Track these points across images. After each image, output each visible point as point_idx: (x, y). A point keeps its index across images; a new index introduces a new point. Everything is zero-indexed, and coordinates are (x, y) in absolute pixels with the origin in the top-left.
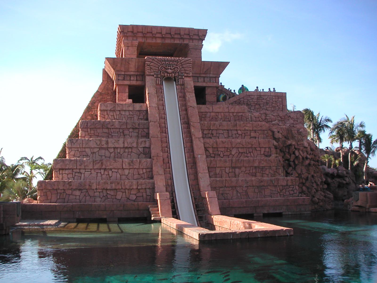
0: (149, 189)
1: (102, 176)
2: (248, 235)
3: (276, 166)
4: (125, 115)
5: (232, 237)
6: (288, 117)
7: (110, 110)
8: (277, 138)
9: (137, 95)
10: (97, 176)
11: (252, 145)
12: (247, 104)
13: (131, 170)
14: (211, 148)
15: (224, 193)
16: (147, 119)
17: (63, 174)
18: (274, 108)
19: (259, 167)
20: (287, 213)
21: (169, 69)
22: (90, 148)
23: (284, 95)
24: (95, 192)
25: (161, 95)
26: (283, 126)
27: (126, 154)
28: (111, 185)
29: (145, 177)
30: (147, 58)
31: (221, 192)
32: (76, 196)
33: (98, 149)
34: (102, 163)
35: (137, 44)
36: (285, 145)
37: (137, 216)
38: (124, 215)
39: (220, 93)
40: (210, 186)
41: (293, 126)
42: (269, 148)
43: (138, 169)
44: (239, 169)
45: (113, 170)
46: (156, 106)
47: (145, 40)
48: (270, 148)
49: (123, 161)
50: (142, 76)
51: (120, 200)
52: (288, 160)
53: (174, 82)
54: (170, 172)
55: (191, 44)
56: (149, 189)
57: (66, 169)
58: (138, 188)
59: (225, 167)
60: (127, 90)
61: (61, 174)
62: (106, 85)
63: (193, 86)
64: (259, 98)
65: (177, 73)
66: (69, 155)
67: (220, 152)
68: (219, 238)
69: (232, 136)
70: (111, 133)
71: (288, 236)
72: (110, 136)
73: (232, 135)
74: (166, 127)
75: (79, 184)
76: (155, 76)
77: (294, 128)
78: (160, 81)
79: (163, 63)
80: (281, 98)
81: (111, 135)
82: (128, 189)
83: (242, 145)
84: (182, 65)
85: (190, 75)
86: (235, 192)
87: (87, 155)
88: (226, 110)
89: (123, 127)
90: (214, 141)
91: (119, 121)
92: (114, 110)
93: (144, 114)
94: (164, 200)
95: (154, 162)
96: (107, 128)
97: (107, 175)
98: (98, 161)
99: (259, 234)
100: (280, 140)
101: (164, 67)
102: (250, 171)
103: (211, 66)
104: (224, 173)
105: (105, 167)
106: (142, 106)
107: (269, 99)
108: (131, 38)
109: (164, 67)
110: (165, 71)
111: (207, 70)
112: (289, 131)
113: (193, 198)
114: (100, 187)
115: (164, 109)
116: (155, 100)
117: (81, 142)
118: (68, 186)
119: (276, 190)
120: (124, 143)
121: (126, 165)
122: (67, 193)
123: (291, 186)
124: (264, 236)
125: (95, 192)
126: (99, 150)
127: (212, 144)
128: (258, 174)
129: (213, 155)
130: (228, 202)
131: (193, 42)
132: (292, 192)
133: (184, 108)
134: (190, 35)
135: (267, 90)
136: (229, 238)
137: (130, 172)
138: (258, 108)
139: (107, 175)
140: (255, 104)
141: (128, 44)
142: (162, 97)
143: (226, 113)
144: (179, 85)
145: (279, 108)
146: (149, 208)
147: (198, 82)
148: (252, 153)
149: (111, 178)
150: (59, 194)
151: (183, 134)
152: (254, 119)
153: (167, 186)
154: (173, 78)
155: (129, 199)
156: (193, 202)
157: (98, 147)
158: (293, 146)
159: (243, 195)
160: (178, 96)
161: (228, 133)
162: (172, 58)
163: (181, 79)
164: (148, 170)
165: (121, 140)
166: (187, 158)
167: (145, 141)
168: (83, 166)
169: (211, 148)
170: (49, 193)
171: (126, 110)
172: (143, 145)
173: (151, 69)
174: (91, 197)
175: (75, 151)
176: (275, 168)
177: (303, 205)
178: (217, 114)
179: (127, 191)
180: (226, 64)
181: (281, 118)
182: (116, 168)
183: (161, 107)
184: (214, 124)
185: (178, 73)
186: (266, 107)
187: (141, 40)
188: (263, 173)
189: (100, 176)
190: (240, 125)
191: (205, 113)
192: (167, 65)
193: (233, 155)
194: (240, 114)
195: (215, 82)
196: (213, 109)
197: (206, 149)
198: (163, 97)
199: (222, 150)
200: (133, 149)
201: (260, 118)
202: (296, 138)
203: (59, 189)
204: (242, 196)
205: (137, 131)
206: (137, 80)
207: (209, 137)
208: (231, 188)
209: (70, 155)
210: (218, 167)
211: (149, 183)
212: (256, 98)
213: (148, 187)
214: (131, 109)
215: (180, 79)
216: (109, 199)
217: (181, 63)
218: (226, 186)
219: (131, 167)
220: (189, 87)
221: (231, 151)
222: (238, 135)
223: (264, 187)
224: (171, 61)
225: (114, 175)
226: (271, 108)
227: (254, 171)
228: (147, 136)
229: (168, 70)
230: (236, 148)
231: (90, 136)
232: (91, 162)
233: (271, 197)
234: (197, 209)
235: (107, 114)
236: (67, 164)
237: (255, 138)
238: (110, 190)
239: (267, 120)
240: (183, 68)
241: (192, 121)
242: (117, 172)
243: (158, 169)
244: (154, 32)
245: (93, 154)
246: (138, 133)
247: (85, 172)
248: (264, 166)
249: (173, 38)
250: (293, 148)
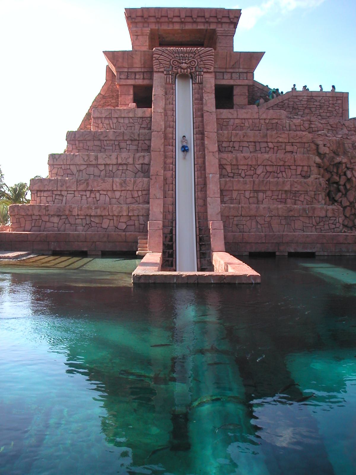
0: (143, 216)
1: (88, 199)
2: (198, 279)
3: (315, 190)
4: (124, 123)
5: (176, 281)
6: (342, 125)
7: (105, 118)
8: (322, 153)
9: (143, 98)
10: (82, 199)
11: (285, 162)
12: (293, 107)
13: (123, 192)
14: (229, 165)
15: (240, 224)
16: (150, 129)
17: (41, 197)
18: (330, 113)
19: (290, 191)
20: (322, 253)
21: (184, 63)
22: (75, 164)
23: (344, 96)
24: (76, 219)
25: (172, 97)
26: (333, 138)
27: (119, 172)
28: (96, 210)
29: (141, 201)
30: (155, 50)
31: (235, 223)
32: (54, 223)
33: (86, 166)
34: (88, 184)
35: (149, 32)
36: (332, 163)
37: (125, 250)
38: (109, 247)
39: (261, 93)
40: (220, 213)
41: (347, 138)
42: (307, 166)
43: (132, 190)
44: (263, 193)
45: (101, 192)
46: (162, 111)
47: (159, 25)
48: (309, 166)
49: (113, 182)
50: (150, 73)
51: (107, 229)
52: (337, 183)
53: (191, 80)
54: (173, 195)
55: (219, 29)
56: (143, 216)
57: (44, 191)
58: (129, 215)
59: (245, 191)
60: (132, 92)
61: (39, 197)
62: (110, 85)
63: (214, 85)
64: (309, 100)
65: (194, 68)
66: (51, 174)
67: (241, 170)
68: (159, 282)
69: (260, 150)
70: (105, 146)
71: (252, 283)
72: (103, 150)
73: (260, 148)
74: (174, 138)
75: (58, 208)
76: (165, 72)
77: (348, 141)
78: (172, 79)
79: (175, 55)
80: (342, 99)
81: (104, 148)
82: (117, 216)
83: (272, 162)
84: (201, 58)
85: (210, 70)
86: (254, 223)
87: (72, 173)
88: (256, 116)
89: (119, 139)
90: (234, 156)
91: (114, 131)
92: (110, 118)
93: (148, 121)
94: (154, 230)
95: (152, 182)
96: (99, 140)
97: (93, 198)
98: (83, 181)
99: (212, 280)
100: (327, 155)
101: (177, 61)
102: (278, 196)
103: (240, 58)
104: (242, 197)
105: (92, 189)
106: (145, 111)
107: (324, 102)
108: (140, 25)
109: (177, 61)
110: (178, 66)
111: (236, 62)
112: (340, 144)
113: (198, 229)
114: (82, 213)
115: (173, 115)
116: (161, 104)
117: (65, 158)
118: (44, 211)
119: (311, 223)
120: (117, 158)
121: (116, 186)
122: (44, 220)
123: (332, 218)
124: (219, 282)
125: (76, 219)
126: (87, 167)
127: (231, 160)
128: (289, 201)
129: (231, 175)
130: (242, 235)
131: (222, 27)
132: (333, 226)
133: (199, 113)
134: (218, 17)
135: (329, 89)
136: (172, 282)
137: (122, 195)
138: (308, 114)
139: (93, 198)
140: (304, 108)
141: (137, 32)
142: (173, 100)
143: (256, 120)
144: (196, 83)
145: (338, 113)
146: (138, 240)
147: (223, 79)
148: (283, 173)
149: (98, 202)
150: (34, 221)
151: (195, 147)
152: (294, 127)
153: (165, 213)
154: (190, 75)
155: (118, 228)
156: (197, 234)
157: (85, 163)
158: (344, 165)
159: (265, 227)
160: (194, 98)
161: (255, 146)
162: (188, 48)
163: (199, 75)
164: (144, 193)
165: (114, 155)
166: (196, 177)
167: (144, 156)
168: (65, 187)
169: (229, 165)
170: (22, 220)
171: (125, 117)
172: (141, 161)
173: (160, 64)
174: (71, 224)
175: (58, 168)
176: (313, 193)
177: (345, 244)
178: (243, 120)
179: (115, 218)
180: (261, 54)
181: (332, 127)
182: (105, 189)
183: (170, 112)
184: (237, 135)
185: (195, 68)
186: (318, 112)
187: (153, 26)
188: (296, 200)
189: (86, 199)
190: (272, 136)
191: (227, 120)
192: (181, 58)
193: (259, 175)
194: (274, 121)
195: (246, 78)
196: (237, 115)
197: (221, 166)
198: (174, 99)
199: (244, 169)
200: (129, 166)
201: (302, 126)
202: (349, 154)
203: (34, 215)
204: (263, 228)
205: (136, 143)
206: (144, 79)
207: (229, 151)
208: (249, 218)
209: (52, 173)
210: (234, 190)
211: (142, 209)
212: (306, 100)
213: (141, 214)
214: (131, 115)
215: (198, 76)
216: (93, 228)
217: (199, 55)
218: (242, 215)
219: (123, 189)
220: (208, 86)
221: (256, 169)
222: (269, 149)
223: (294, 218)
224: (186, 52)
225: (103, 197)
226: (326, 113)
227: (284, 196)
228: (148, 149)
229: (182, 64)
230: (263, 166)
231: (79, 150)
232: (75, 182)
233: (303, 231)
234: (200, 243)
235: (102, 123)
236: (46, 185)
237: (291, 153)
238: (95, 216)
239: (311, 129)
240: (202, 61)
241: (207, 130)
242: (106, 195)
243: (156, 192)
244: (171, 15)
245: (79, 173)
246: (138, 145)
247: (68, 194)
248: (298, 190)
249: (195, 22)
250: (343, 167)
